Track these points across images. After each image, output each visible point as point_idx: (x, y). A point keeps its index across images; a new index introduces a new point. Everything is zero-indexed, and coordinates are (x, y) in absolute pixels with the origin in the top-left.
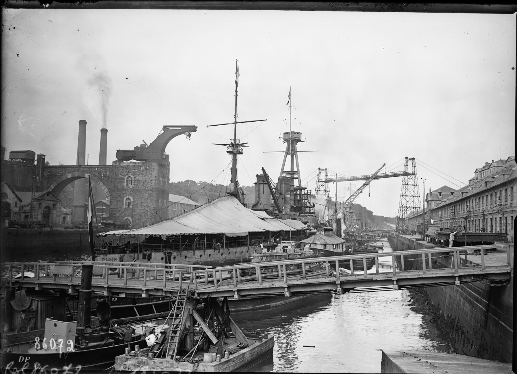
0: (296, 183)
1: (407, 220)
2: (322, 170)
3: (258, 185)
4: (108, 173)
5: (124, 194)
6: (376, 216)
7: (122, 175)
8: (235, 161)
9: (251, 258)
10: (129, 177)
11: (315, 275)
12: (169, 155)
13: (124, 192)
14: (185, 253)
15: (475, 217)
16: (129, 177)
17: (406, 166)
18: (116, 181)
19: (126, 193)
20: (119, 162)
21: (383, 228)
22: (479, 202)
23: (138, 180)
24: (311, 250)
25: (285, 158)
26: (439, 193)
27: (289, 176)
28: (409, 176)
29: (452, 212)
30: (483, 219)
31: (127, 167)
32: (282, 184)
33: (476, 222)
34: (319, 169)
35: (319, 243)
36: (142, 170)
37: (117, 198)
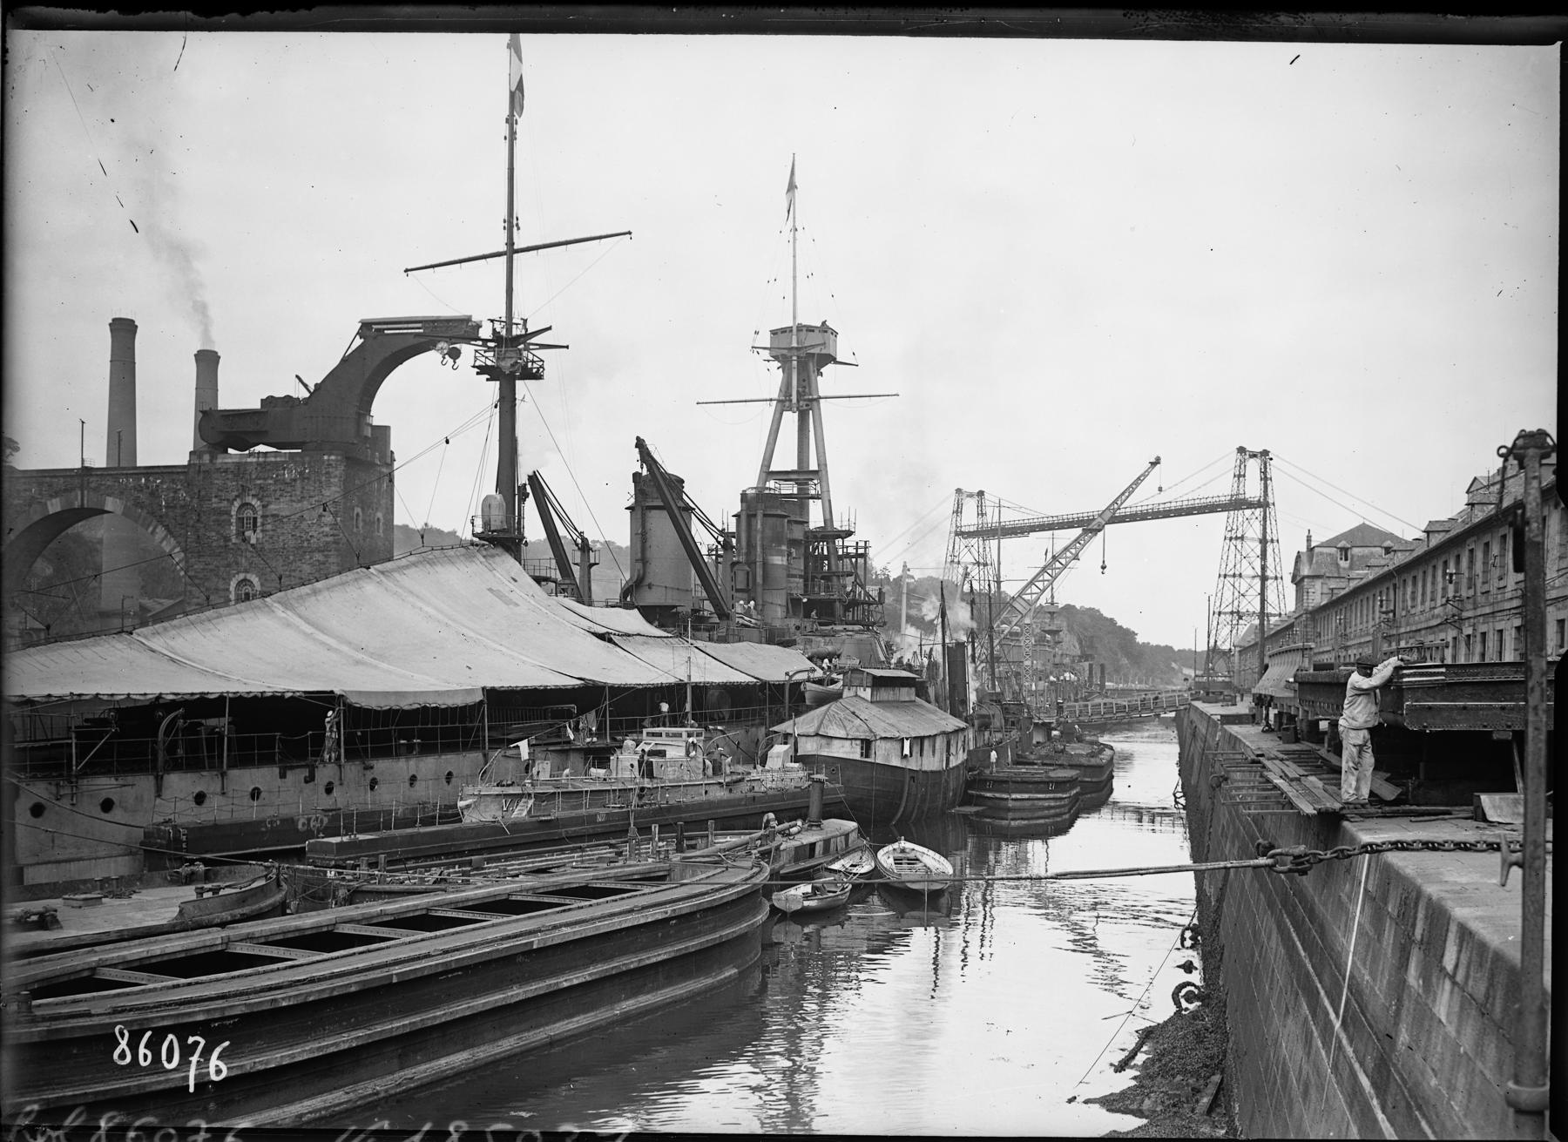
0: (816, 519)
1: (1237, 654)
2: (968, 496)
3: (639, 513)
4: (182, 494)
5: (229, 565)
6: (1146, 645)
7: (221, 500)
8: (507, 405)
9: (461, 804)
10: (248, 504)
11: (620, 913)
12: (387, 428)
13: (231, 558)
14: (105, 785)
15: (1481, 619)
16: (245, 505)
17: (1239, 476)
18: (204, 518)
19: (237, 564)
20: (210, 453)
21: (1167, 684)
22: (1503, 555)
23: (273, 515)
24: (797, 765)
25: (775, 424)
26: (1341, 549)
27: (789, 489)
28: (1248, 512)
29: (1384, 609)
30: (1518, 628)
31: (239, 469)
32: (755, 515)
33: (1484, 641)
34: (959, 491)
35: (842, 734)
36: (288, 481)
37: (208, 579)
